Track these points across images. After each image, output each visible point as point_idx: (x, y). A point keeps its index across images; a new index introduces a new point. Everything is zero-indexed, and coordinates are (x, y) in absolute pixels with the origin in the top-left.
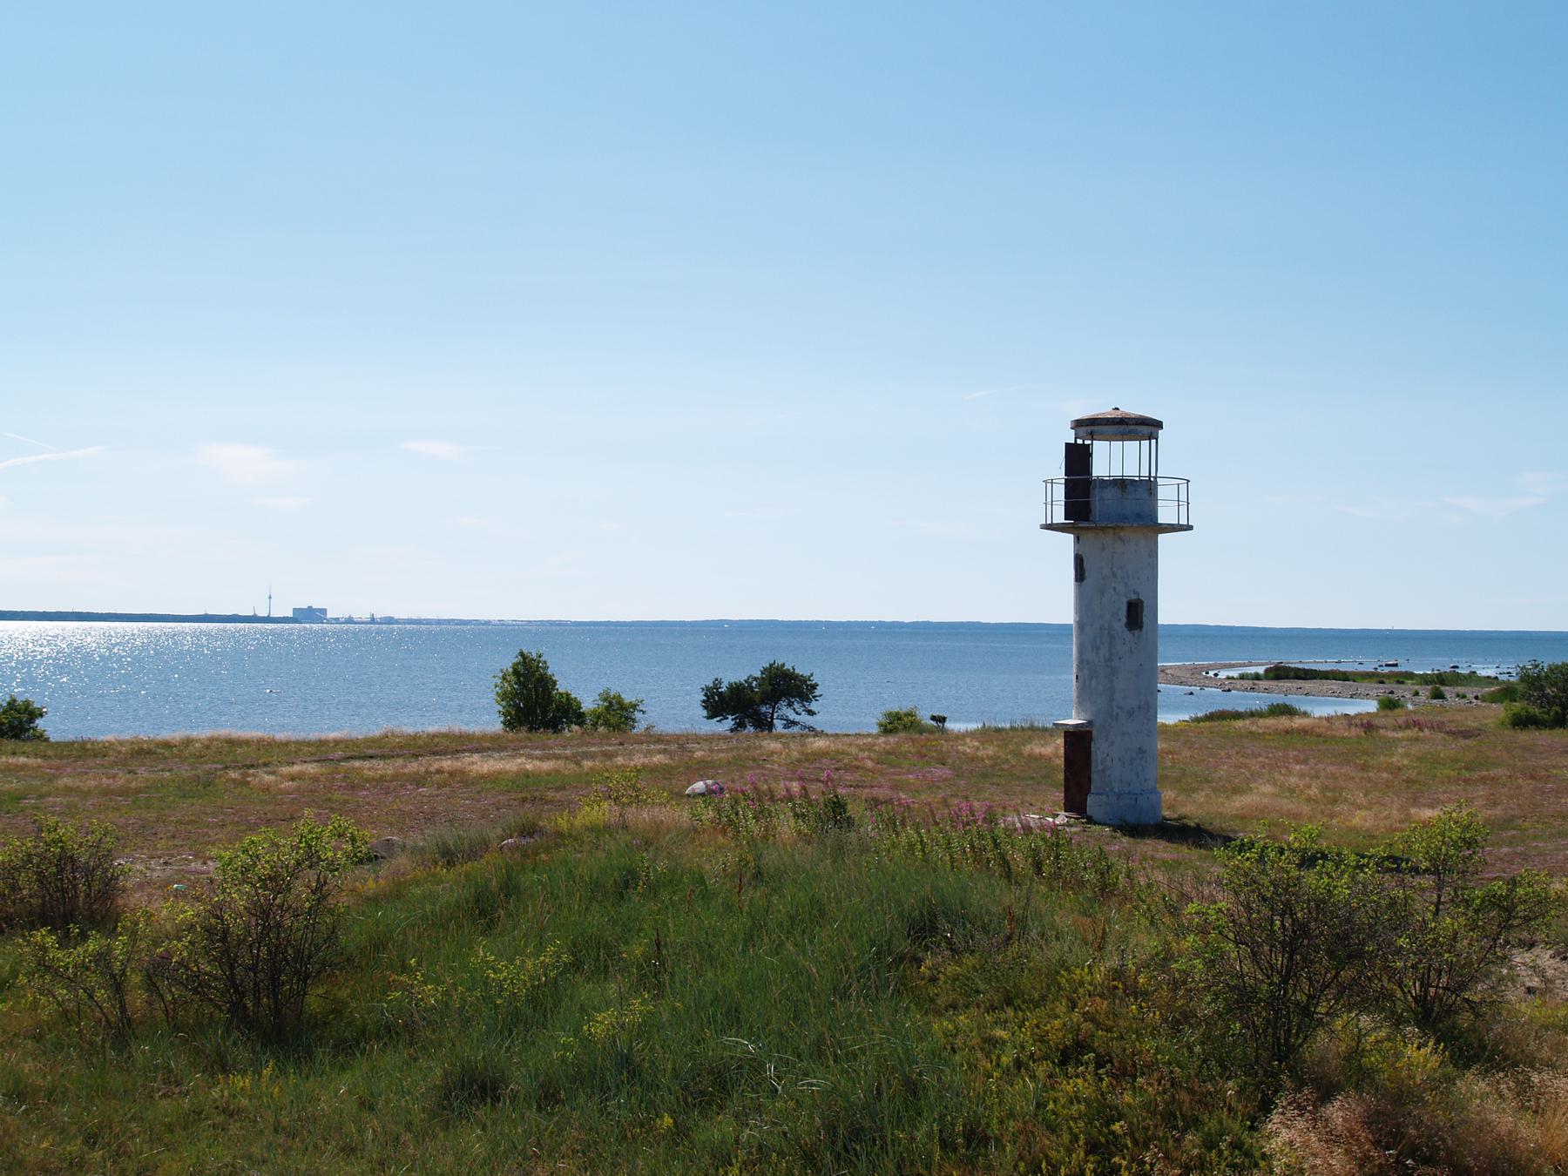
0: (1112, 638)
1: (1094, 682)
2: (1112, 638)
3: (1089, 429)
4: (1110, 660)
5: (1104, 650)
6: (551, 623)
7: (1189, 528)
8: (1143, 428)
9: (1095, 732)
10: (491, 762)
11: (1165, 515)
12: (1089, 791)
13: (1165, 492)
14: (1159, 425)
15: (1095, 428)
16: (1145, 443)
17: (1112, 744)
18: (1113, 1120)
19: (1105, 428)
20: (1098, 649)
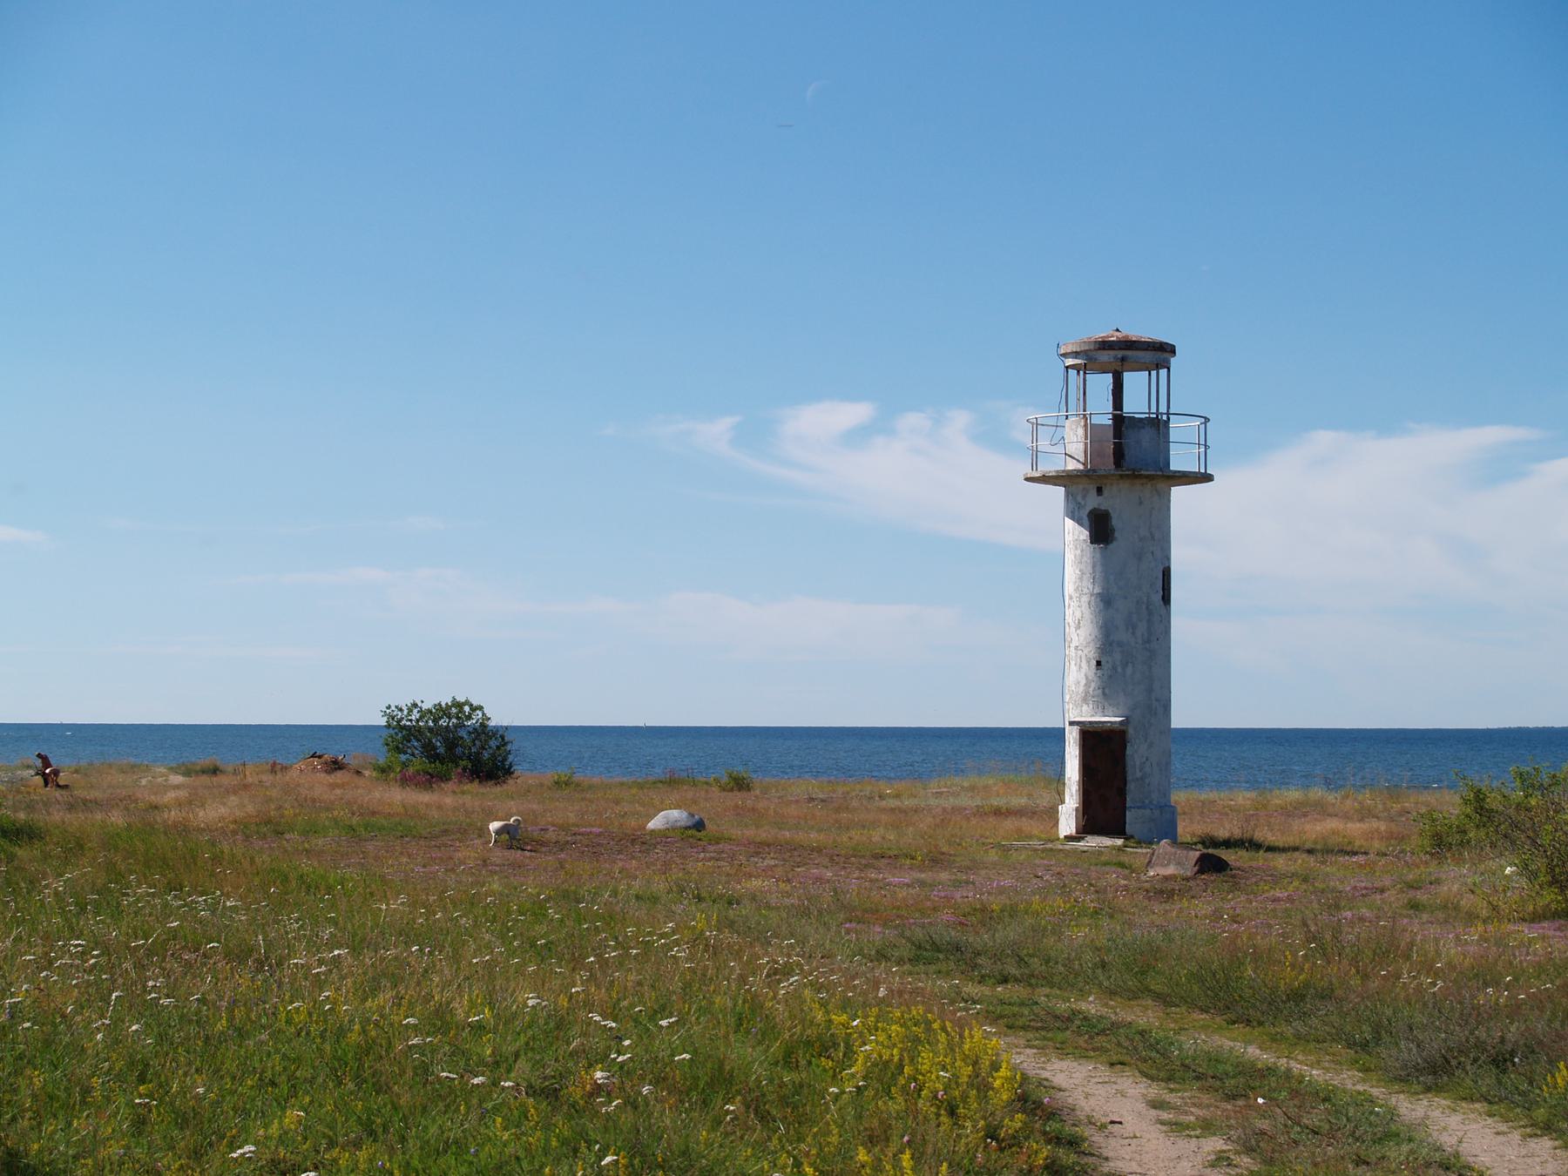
0: (1150, 613)
1: (1129, 670)
2: (1150, 613)
3: (1120, 354)
4: (1149, 641)
5: (1142, 628)
6: (1520, 729)
7: (1207, 478)
8: (1158, 354)
9: (1131, 731)
10: (1142, 1023)
11: (1180, 460)
12: (1124, 809)
13: (1179, 429)
14: (1166, 349)
15: (1129, 353)
16: (1154, 373)
17: (1151, 745)
18: (579, 902)
19: (1140, 354)
20: (1134, 627)
